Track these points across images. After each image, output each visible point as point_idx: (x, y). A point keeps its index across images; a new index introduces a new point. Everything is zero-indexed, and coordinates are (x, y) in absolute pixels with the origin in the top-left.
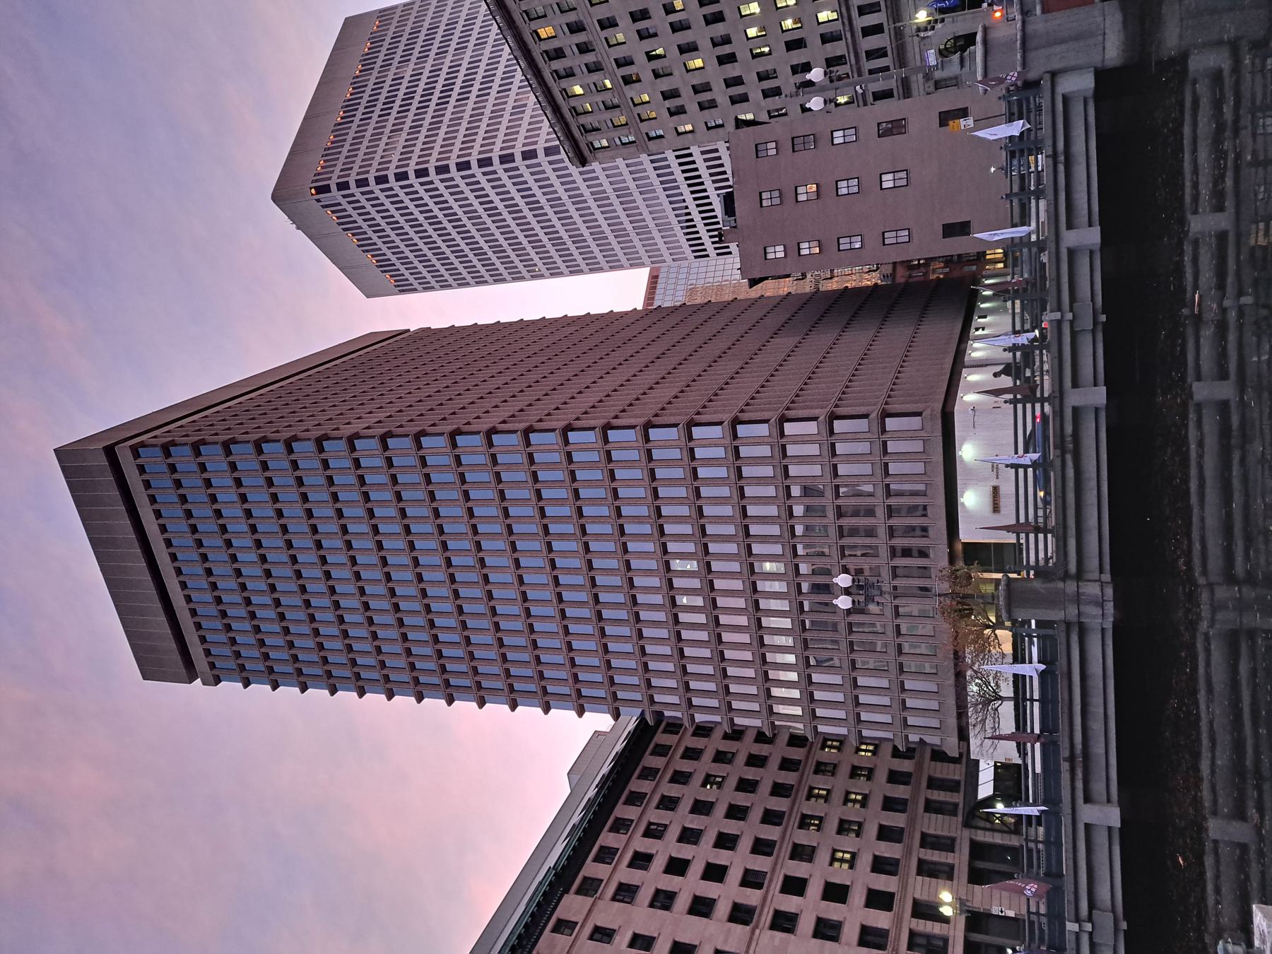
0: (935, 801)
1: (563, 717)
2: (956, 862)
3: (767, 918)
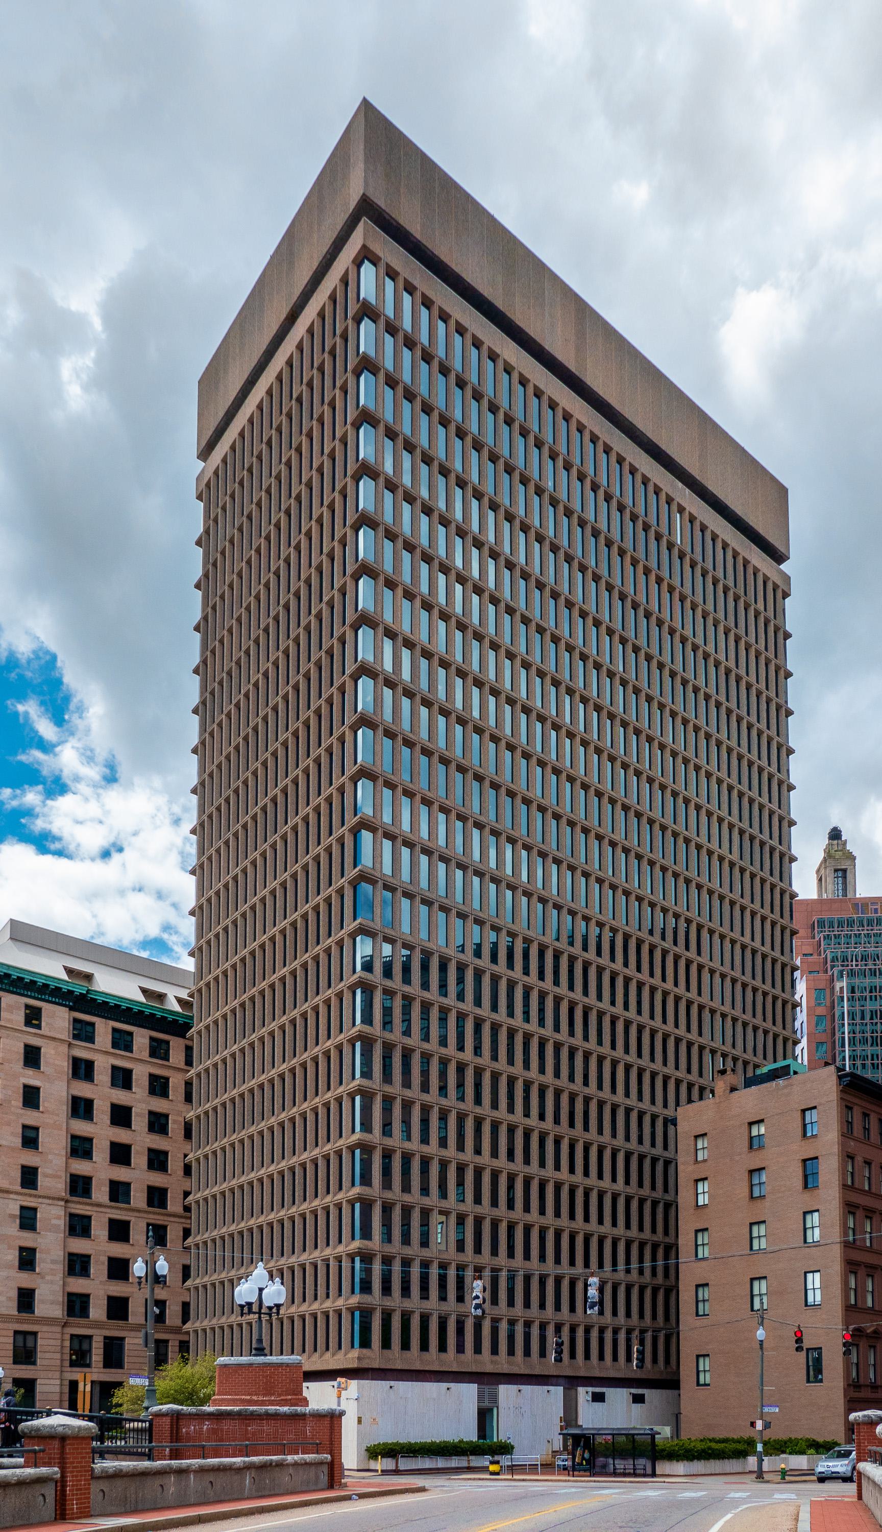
0: (167, 1347)
2: (94, 1370)
3: (80, 1209)
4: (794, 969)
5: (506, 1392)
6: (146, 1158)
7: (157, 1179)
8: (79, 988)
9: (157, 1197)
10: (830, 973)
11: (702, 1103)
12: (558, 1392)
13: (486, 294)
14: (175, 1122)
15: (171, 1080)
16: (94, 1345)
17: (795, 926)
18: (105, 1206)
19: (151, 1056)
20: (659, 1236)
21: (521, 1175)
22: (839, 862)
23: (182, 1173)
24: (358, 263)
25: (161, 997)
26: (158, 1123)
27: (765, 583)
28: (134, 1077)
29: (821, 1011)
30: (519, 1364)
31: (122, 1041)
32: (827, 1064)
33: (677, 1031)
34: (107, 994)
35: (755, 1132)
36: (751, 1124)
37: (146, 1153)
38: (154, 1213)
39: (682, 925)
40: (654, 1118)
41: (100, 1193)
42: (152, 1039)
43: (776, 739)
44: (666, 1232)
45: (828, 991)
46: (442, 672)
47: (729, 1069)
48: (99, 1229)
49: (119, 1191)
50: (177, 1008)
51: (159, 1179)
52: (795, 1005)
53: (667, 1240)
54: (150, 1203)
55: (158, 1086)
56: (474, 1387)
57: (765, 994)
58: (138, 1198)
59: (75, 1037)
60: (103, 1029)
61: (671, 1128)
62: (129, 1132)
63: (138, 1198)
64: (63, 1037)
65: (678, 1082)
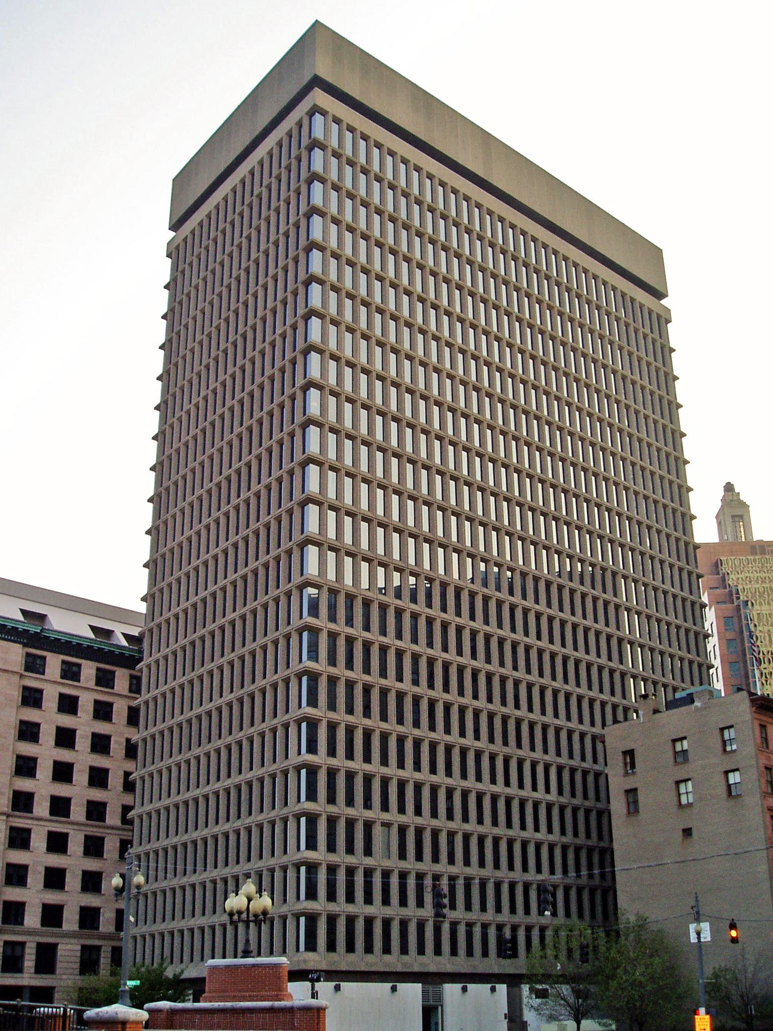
0: (99, 955)
1: (141, 582)
2: (26, 975)
3: (20, 822)
4: (703, 606)
5: (451, 990)
6: (87, 776)
7: (97, 795)
8: (34, 628)
9: (96, 811)
10: (736, 603)
11: (627, 723)
12: (502, 988)
13: (411, 131)
14: (116, 742)
15: (115, 706)
16: (27, 951)
17: (700, 571)
18: (46, 820)
19: (96, 685)
20: (594, 841)
21: (459, 789)
22: (733, 509)
23: (122, 789)
24: (311, 114)
25: (108, 633)
26: (100, 744)
27: (650, 314)
28: (80, 703)
29: (729, 635)
30: (461, 964)
31: (71, 673)
32: (739, 690)
33: (599, 660)
34: (60, 632)
35: (678, 747)
36: (674, 741)
37: (88, 770)
38: (92, 826)
39: (598, 572)
40: (582, 736)
41: (41, 808)
42: (98, 669)
43: (670, 426)
44: (600, 837)
45: (736, 620)
46: (348, 336)
47: (650, 694)
48: (39, 841)
49: (60, 806)
50: (124, 643)
51: (98, 795)
52: (703, 606)
53: (602, 844)
54: (89, 816)
55: (103, 711)
56: (419, 986)
57: (678, 627)
58: (78, 812)
59: (26, 670)
60: (54, 662)
61: (599, 746)
62: (73, 753)
63: (78, 812)
64: (15, 669)
65: (603, 704)
